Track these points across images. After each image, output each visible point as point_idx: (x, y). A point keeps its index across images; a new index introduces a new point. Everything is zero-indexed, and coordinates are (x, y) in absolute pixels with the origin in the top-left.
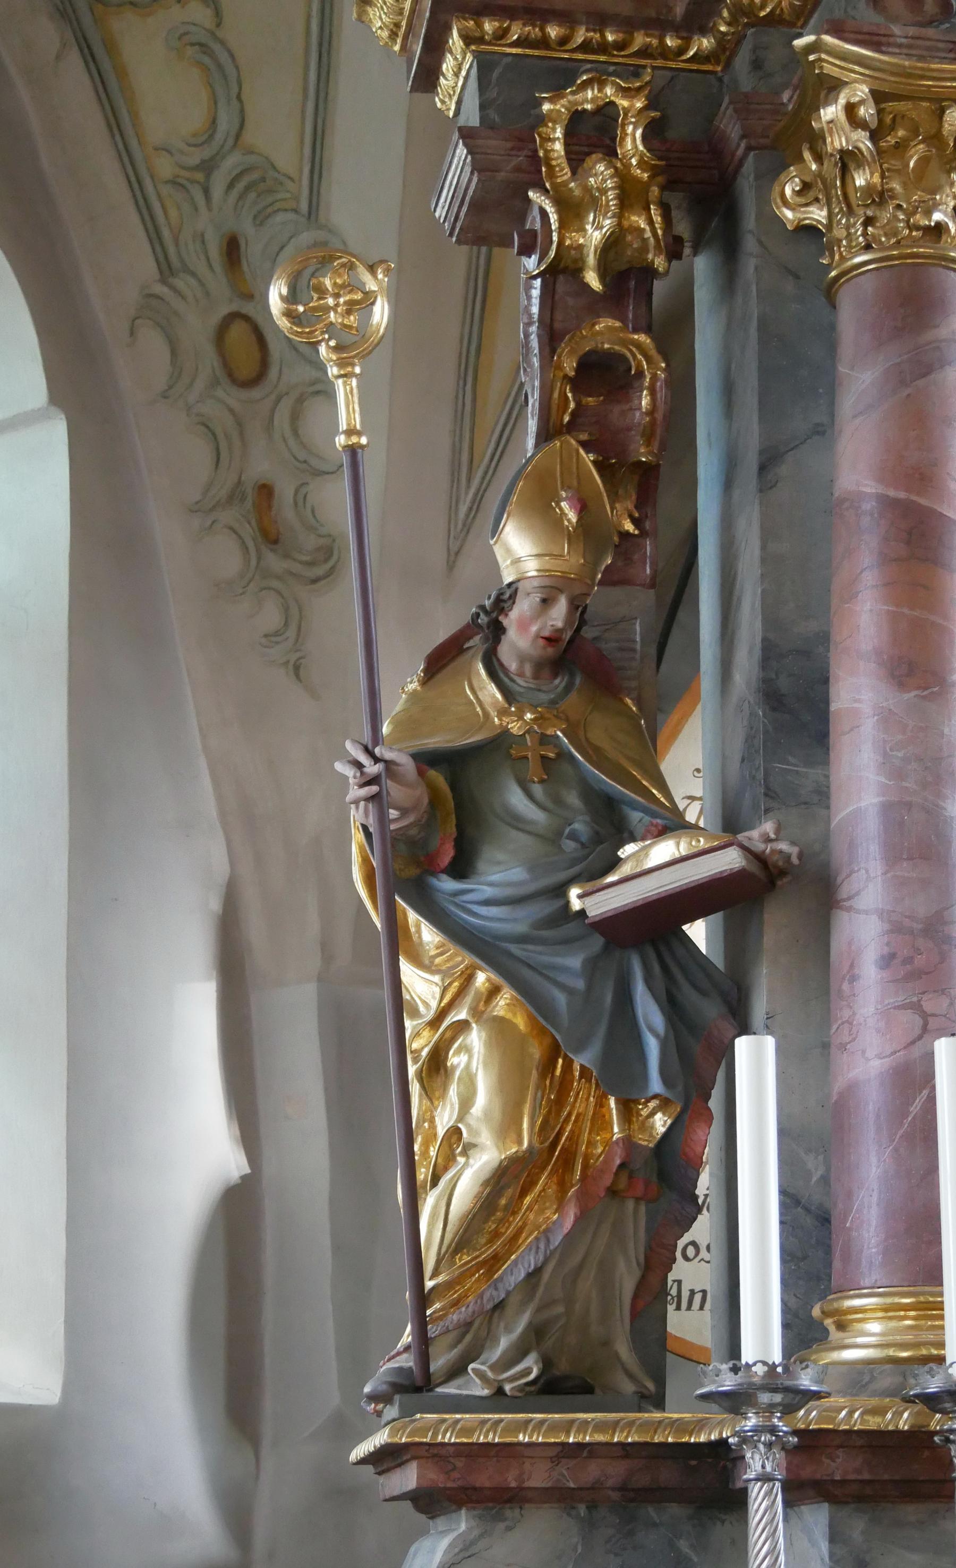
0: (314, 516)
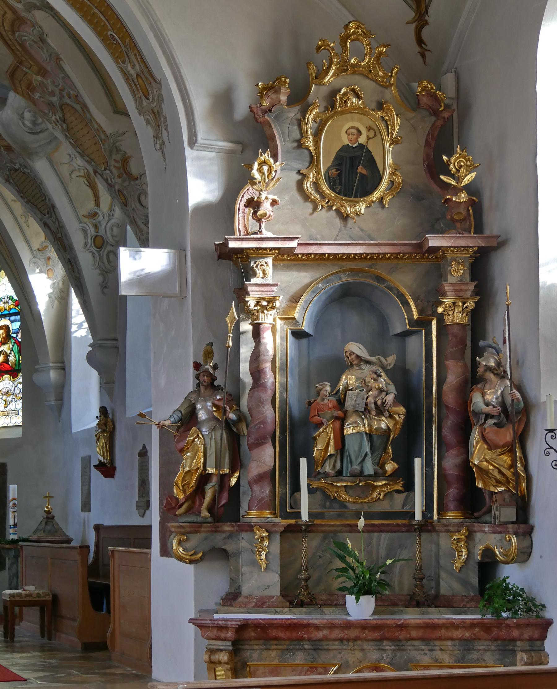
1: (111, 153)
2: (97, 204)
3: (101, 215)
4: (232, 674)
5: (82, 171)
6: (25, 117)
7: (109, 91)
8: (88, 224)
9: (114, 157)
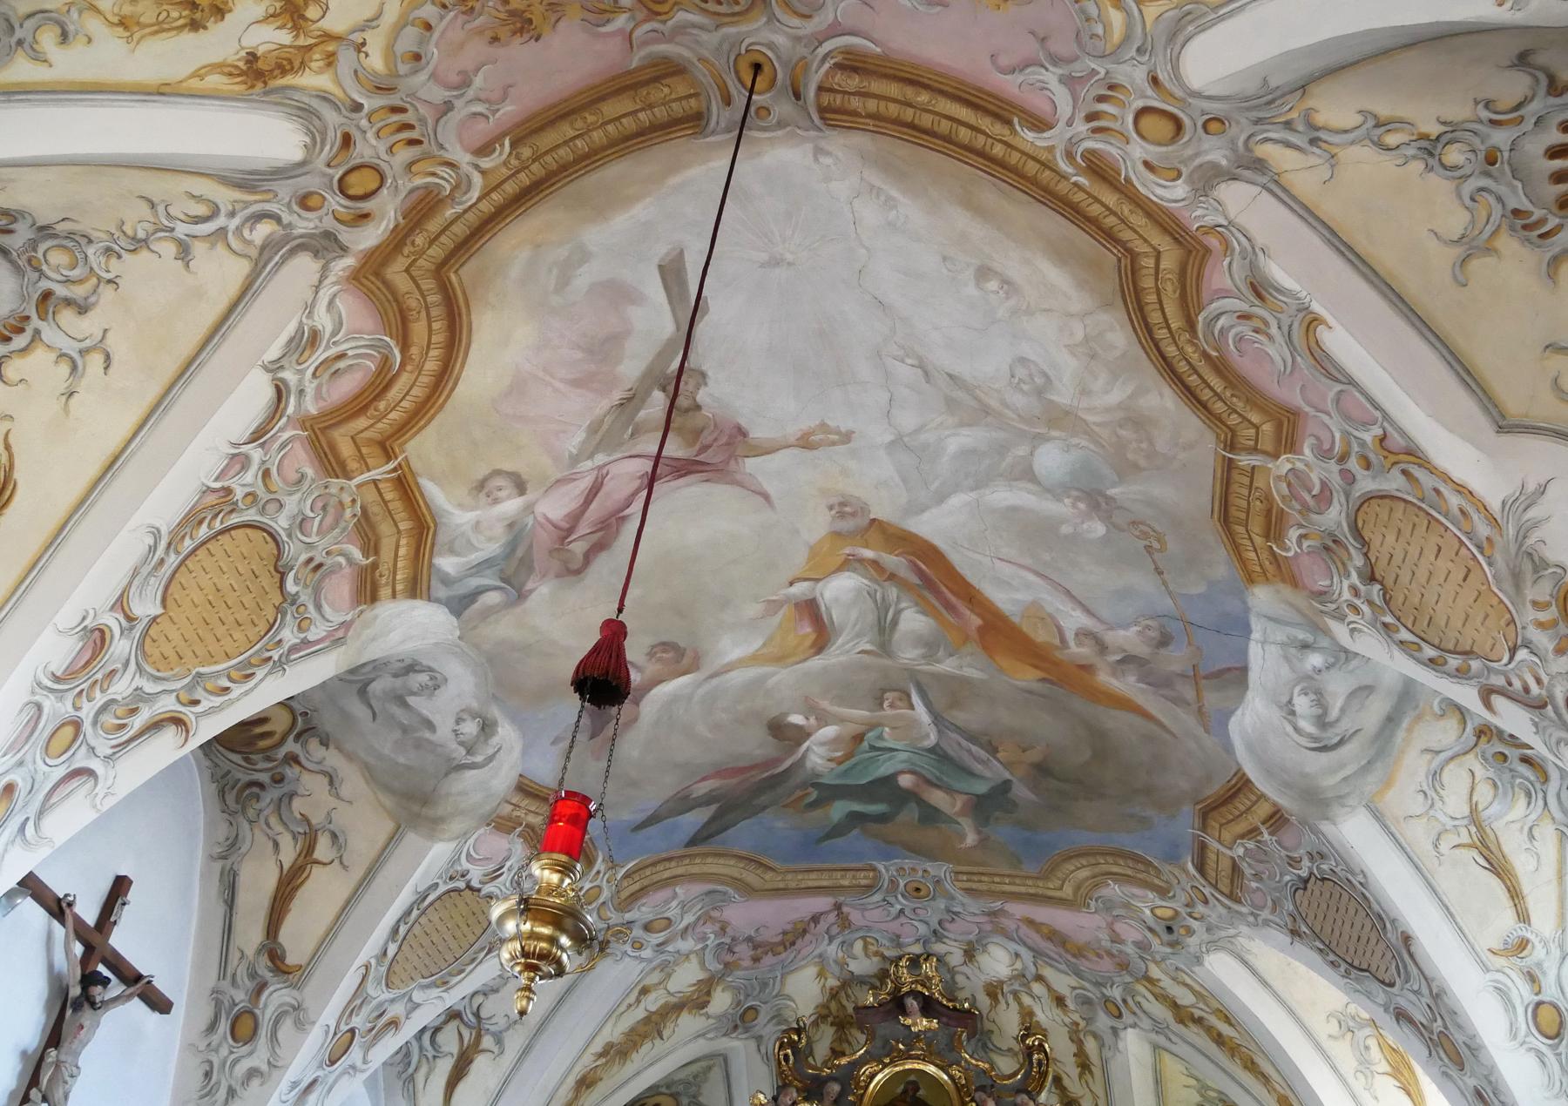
0: (1346, 131)
1: (1517, 578)
2: (1523, 917)
3: (1539, 946)
4: (515, 491)
5: (1464, 831)
6: (1298, 709)
7: (1469, 373)
8: (1508, 971)
9: (1530, 593)
